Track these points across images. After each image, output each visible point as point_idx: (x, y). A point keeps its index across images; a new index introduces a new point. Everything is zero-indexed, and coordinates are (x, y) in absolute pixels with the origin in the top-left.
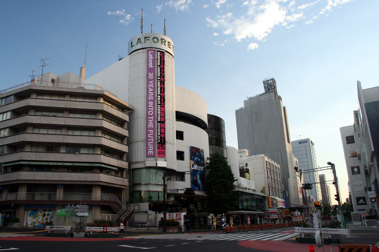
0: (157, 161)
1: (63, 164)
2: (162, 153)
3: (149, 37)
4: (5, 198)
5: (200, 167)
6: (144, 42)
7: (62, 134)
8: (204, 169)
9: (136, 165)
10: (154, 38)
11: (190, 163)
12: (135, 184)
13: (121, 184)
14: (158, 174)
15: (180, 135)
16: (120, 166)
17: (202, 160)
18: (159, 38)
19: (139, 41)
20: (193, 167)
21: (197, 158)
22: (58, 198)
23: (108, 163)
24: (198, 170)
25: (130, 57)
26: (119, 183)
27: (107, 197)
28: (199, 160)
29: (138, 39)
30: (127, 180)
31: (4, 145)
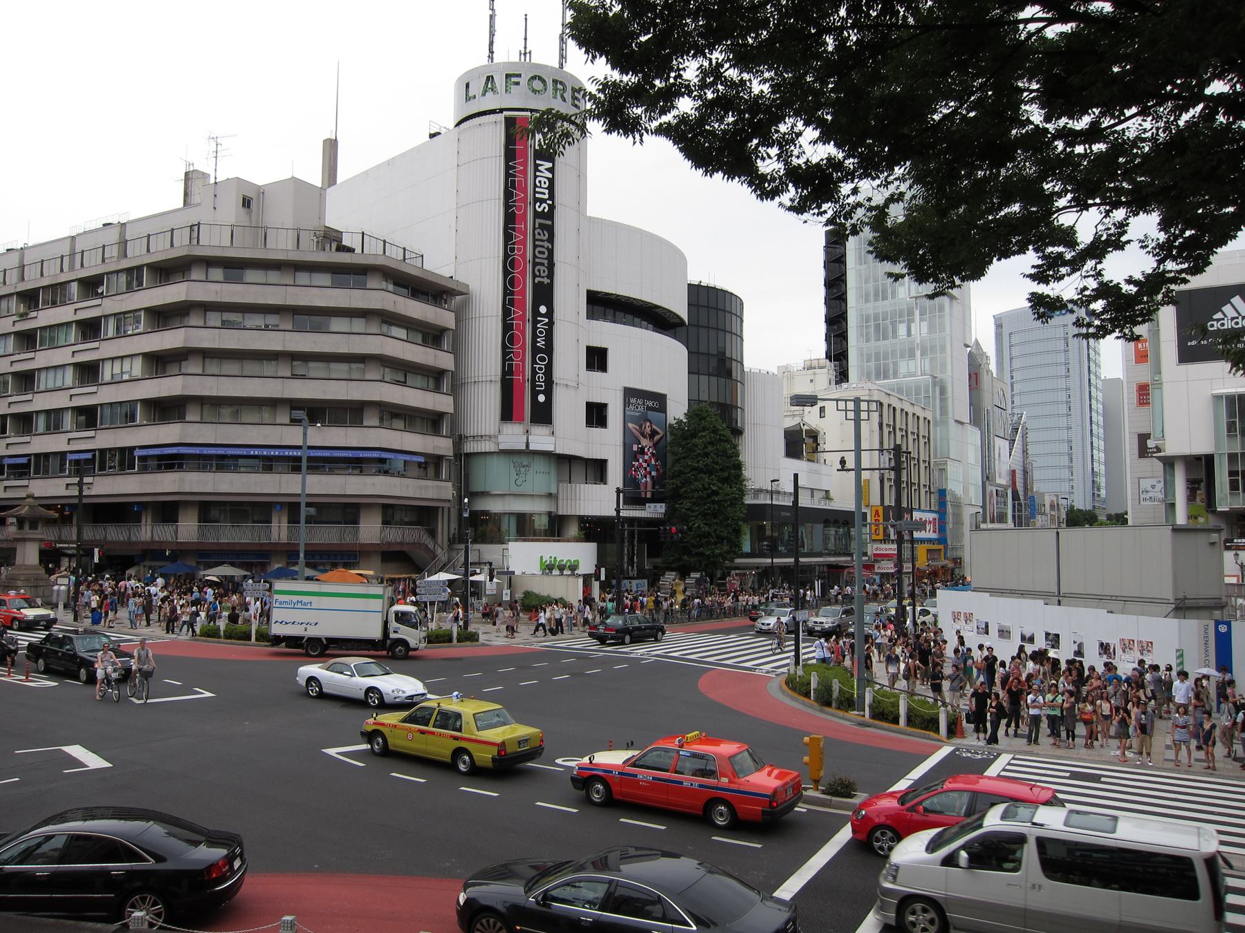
0: (530, 437)
1: (284, 452)
2: (543, 415)
3: (519, 76)
4: (149, 534)
7: (280, 374)
10: (534, 78)
14: (531, 470)
15: (597, 359)
16: (430, 451)
19: (490, 86)
22: (274, 538)
25: (459, 133)
26: (430, 496)
27: (395, 535)
29: (488, 78)
30: (450, 484)
31: (131, 356)
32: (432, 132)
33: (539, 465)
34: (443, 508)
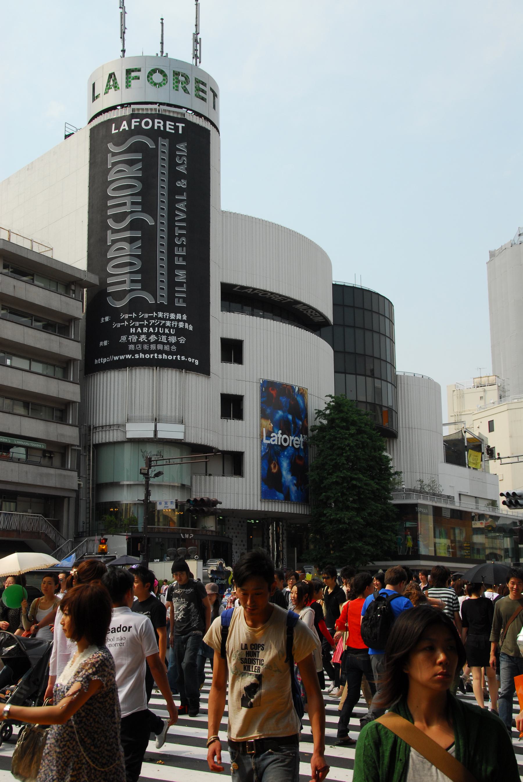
3: (139, 70)
5: (292, 438)
6: (124, 84)
8: (305, 444)
9: (104, 436)
10: (154, 71)
11: (261, 426)
12: (103, 484)
13: (58, 486)
16: (53, 438)
17: (301, 419)
18: (167, 72)
19: (112, 83)
20: (269, 437)
21: (284, 412)
23: (17, 433)
24: (285, 445)
28: (290, 417)
32: (67, 134)
33: (174, 453)
34: (69, 498)
